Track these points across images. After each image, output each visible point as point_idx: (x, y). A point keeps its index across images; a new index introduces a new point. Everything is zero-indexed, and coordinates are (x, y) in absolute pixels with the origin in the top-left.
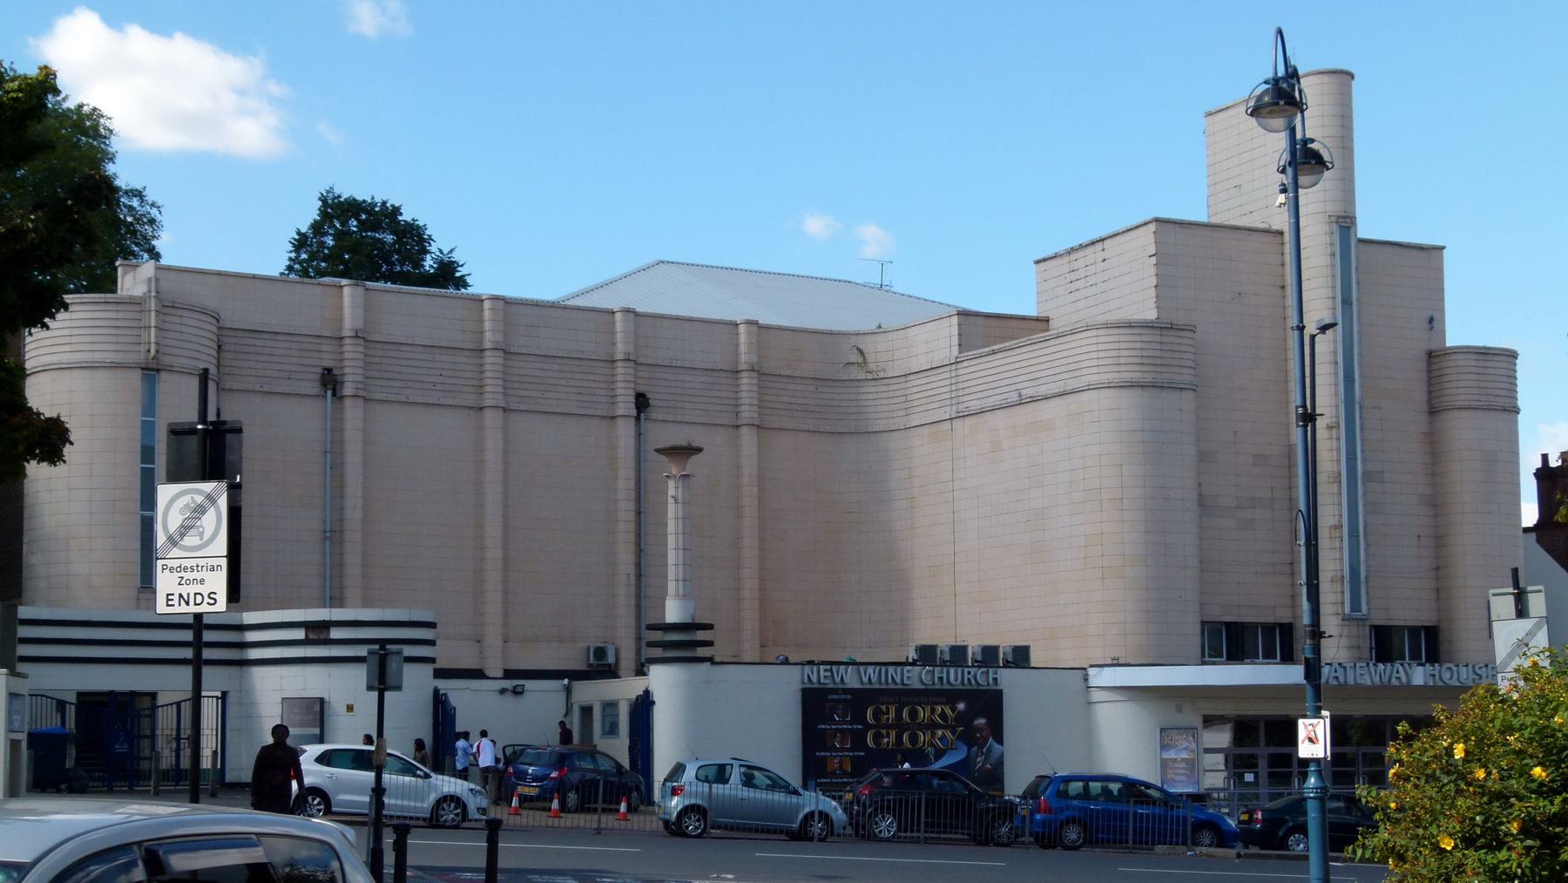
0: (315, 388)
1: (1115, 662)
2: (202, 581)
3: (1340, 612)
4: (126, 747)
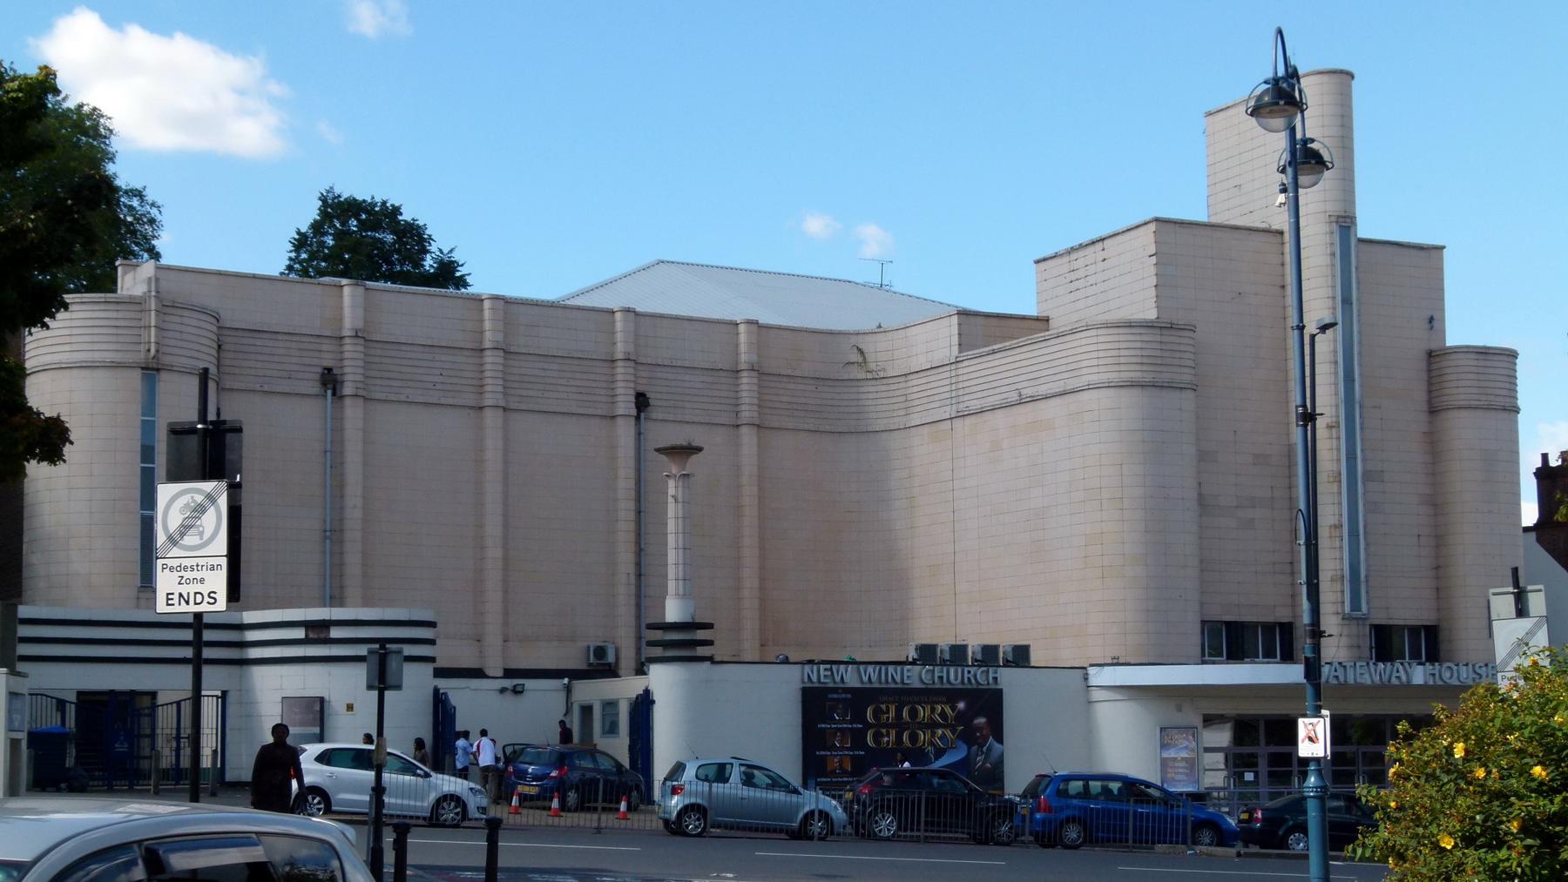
0: (315, 388)
1: (1115, 661)
2: (202, 581)
3: (1340, 611)
4: (126, 746)
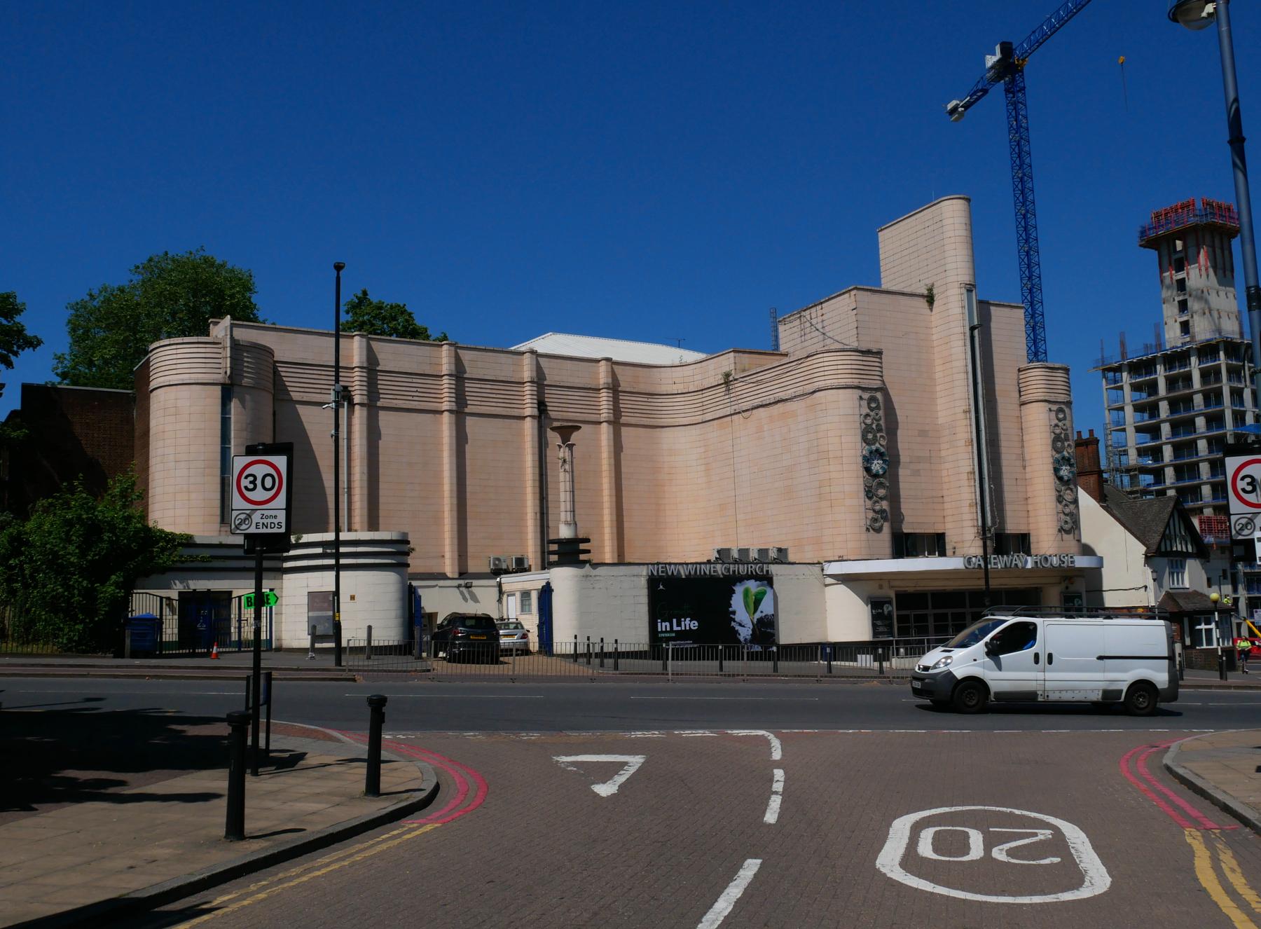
1: (840, 559)
2: (275, 517)
